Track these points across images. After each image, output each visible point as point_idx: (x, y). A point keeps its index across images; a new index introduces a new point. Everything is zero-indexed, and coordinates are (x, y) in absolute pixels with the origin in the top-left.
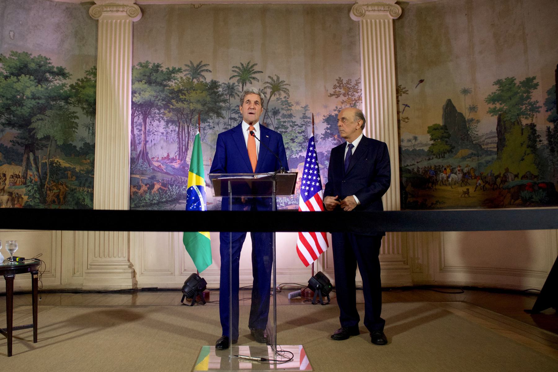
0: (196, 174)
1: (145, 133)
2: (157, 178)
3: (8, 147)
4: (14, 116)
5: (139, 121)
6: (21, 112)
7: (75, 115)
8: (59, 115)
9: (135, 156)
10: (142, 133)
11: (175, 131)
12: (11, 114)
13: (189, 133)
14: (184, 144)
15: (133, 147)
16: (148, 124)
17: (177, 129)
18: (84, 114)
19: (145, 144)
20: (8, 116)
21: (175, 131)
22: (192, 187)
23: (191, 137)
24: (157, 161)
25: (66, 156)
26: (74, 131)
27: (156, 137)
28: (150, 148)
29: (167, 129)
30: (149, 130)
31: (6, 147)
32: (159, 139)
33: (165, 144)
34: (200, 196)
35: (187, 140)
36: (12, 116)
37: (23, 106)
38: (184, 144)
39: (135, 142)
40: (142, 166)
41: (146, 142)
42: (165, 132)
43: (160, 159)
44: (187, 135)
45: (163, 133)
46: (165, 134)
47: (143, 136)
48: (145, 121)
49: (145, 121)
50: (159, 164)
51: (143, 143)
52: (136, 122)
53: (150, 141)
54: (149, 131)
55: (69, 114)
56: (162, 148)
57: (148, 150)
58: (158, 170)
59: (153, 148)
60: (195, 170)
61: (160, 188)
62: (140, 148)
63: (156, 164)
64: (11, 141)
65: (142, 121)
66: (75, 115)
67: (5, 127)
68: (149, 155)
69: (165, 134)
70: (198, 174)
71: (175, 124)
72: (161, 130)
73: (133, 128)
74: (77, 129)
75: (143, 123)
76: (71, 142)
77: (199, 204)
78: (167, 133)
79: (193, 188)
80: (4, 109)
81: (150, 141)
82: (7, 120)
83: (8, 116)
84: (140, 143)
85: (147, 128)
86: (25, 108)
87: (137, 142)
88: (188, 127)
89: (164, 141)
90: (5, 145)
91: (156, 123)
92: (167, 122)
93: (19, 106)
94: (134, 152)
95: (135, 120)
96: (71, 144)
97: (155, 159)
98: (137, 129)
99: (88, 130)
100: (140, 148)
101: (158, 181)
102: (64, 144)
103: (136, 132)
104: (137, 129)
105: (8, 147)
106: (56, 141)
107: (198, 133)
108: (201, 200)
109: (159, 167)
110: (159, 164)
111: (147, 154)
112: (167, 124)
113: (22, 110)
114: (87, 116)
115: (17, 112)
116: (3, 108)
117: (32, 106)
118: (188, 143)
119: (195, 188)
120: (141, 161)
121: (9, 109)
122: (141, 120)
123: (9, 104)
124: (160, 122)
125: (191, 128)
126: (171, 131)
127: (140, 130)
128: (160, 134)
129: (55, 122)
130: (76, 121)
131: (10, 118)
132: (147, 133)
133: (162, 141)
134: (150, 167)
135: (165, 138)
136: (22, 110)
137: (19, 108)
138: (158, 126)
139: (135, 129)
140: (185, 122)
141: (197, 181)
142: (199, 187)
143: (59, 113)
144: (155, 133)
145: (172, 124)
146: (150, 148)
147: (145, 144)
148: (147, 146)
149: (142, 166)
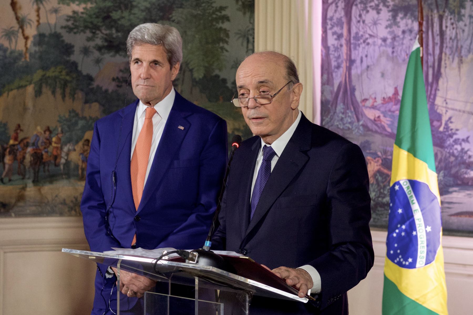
0: (409, 151)
1: (349, 42)
2: (372, 146)
3: (110, 91)
4: (117, 31)
5: (337, 15)
6: (129, 20)
7: (224, 13)
8: (195, 16)
9: (329, 97)
10: (343, 41)
11: (411, 31)
12: (112, 27)
13: (442, 33)
14: (430, 63)
15: (325, 76)
16: (354, 20)
17: (416, 26)
18: (239, 10)
19: (349, 69)
20: (108, 32)
21: (411, 31)
22: (398, 183)
23: (448, 43)
24: (373, 107)
25: (210, 101)
26: (222, 48)
27: (371, 49)
28: (360, 76)
29: (395, 28)
30: (357, 33)
31: (106, 91)
32: (377, 54)
33: (389, 66)
34: (415, 207)
35: (437, 52)
36: (114, 31)
37: (133, 7)
38: (430, 63)
39: (329, 63)
40: (342, 119)
41: (351, 62)
42: (389, 37)
43: (379, 101)
44: (438, 39)
45: (384, 40)
46: (389, 41)
47: (344, 49)
48: (348, 13)
49: (348, 13)
50: (377, 113)
51: (344, 65)
52: (331, 19)
53: (358, 61)
54: (357, 38)
55: (213, 13)
56: (383, 75)
57: (355, 82)
58: (374, 128)
59: (365, 75)
60: (406, 142)
61: (379, 171)
62: (338, 78)
63: (371, 114)
64: (114, 79)
65: (343, 13)
66: (224, 13)
67: (103, 54)
68: (357, 94)
69: (389, 41)
70: (413, 151)
71: (412, 15)
72: (382, 31)
73: (325, 31)
74: (227, 42)
75: (344, 20)
76: (217, 72)
77: (412, 227)
78: (394, 39)
79: (401, 187)
80: (100, 20)
81: (358, 61)
82: (106, 40)
83: (108, 32)
84: (338, 67)
85: (354, 30)
86: (135, 11)
87: (334, 64)
88: (441, 18)
89: (388, 58)
90: (104, 89)
91: (371, 16)
92: (395, 11)
93: (126, 8)
94: (328, 88)
95: (330, 14)
96: (217, 76)
97: (369, 103)
98: (334, 33)
99: (245, 44)
100: (338, 78)
101: (375, 155)
102: (205, 76)
103: (332, 41)
104: (334, 33)
105: (110, 91)
106: (191, 71)
107: (416, 45)
108: (418, 216)
109: (376, 121)
110: (377, 113)
111: (353, 90)
112: (394, 17)
113: (132, 17)
114: (244, 13)
115: (122, 22)
116: (97, 17)
117: (148, 5)
118: (440, 60)
119: (406, 186)
120: (340, 107)
121: (108, 17)
122: (341, 13)
123: (109, 7)
124: (378, 13)
125: (447, 22)
126: (404, 32)
127: (339, 37)
128: (380, 42)
129: (189, 33)
130: (226, 25)
131: (111, 35)
132: (353, 41)
133: (383, 60)
134: (358, 120)
135: (390, 50)
136: (132, 17)
137: (126, 14)
138: (375, 23)
139: (329, 33)
140: (434, 7)
141: (411, 168)
142: (414, 184)
143: (195, 12)
144: (370, 41)
145: (405, 15)
146: (360, 76)
147: (349, 69)
148: (353, 72)
149: (342, 119)
